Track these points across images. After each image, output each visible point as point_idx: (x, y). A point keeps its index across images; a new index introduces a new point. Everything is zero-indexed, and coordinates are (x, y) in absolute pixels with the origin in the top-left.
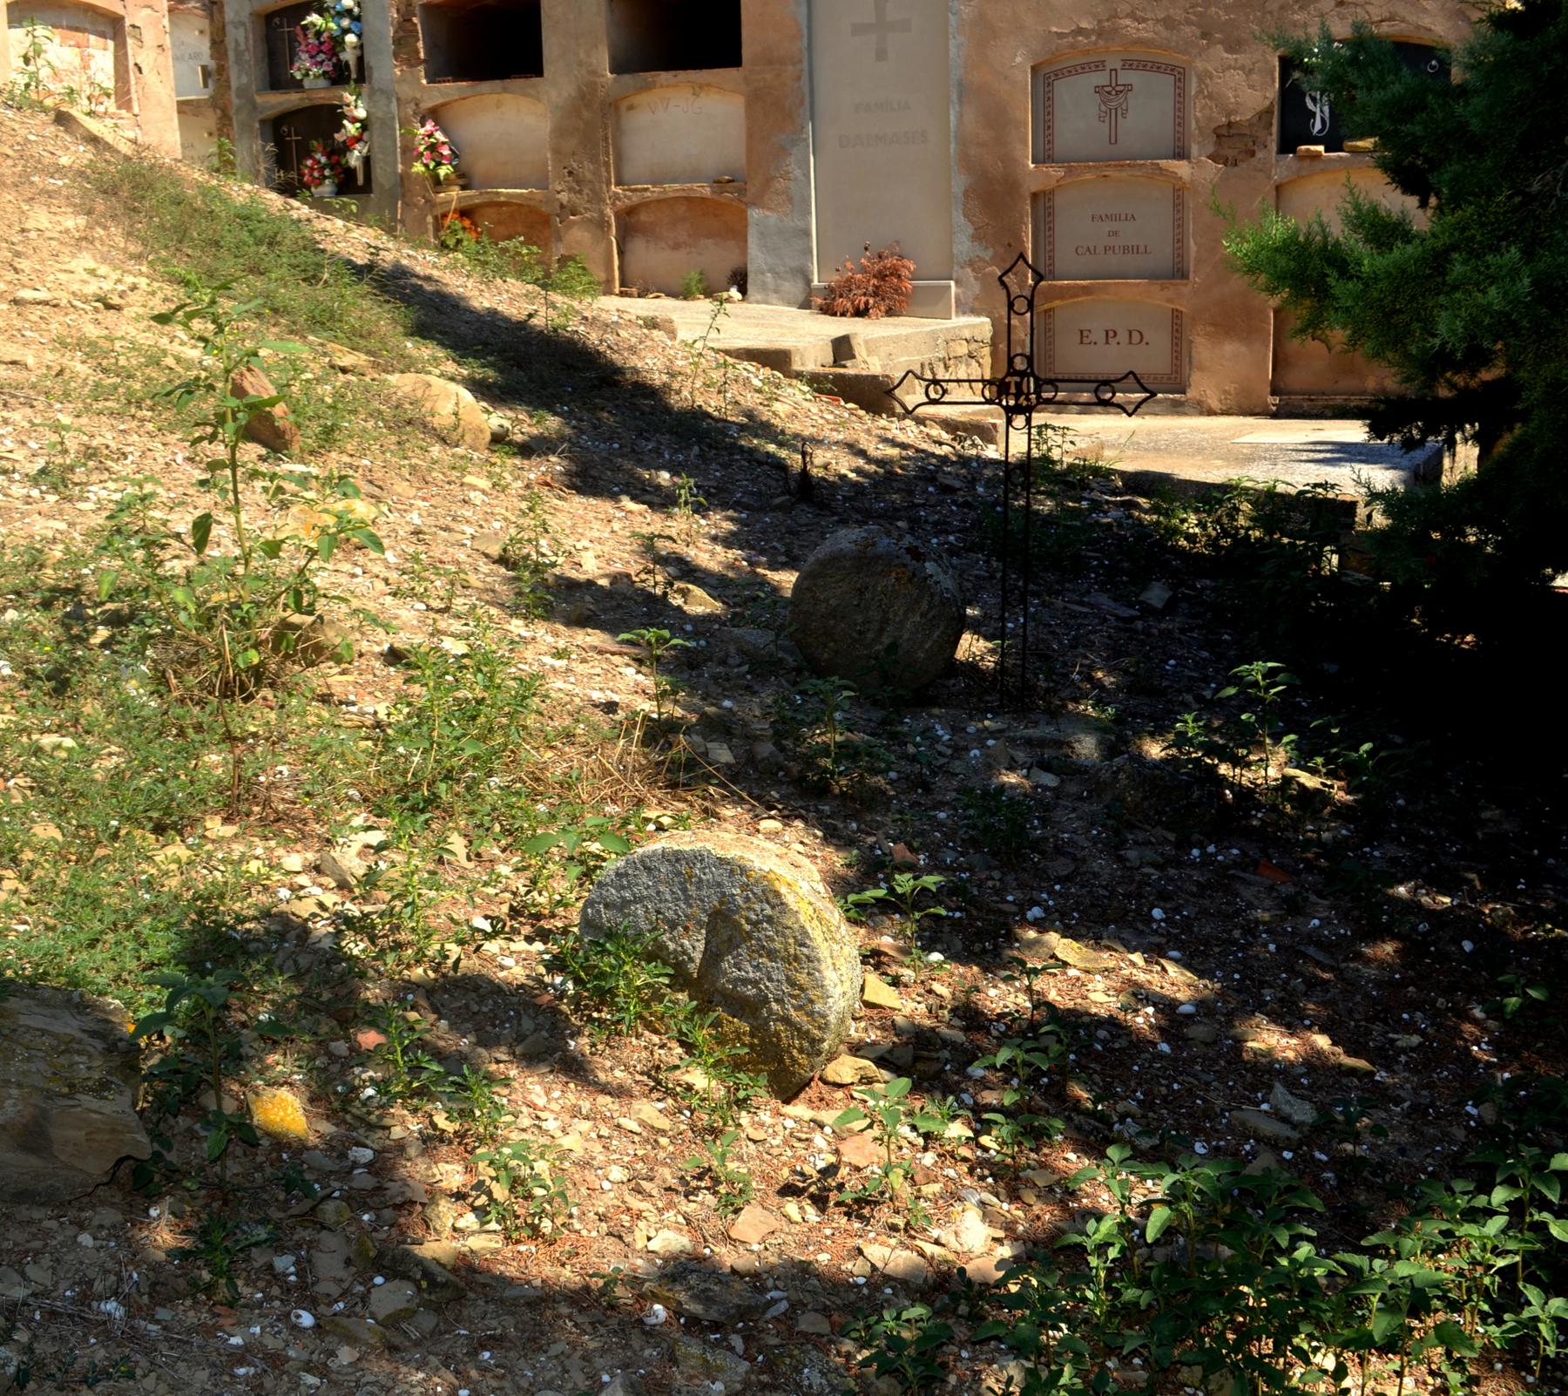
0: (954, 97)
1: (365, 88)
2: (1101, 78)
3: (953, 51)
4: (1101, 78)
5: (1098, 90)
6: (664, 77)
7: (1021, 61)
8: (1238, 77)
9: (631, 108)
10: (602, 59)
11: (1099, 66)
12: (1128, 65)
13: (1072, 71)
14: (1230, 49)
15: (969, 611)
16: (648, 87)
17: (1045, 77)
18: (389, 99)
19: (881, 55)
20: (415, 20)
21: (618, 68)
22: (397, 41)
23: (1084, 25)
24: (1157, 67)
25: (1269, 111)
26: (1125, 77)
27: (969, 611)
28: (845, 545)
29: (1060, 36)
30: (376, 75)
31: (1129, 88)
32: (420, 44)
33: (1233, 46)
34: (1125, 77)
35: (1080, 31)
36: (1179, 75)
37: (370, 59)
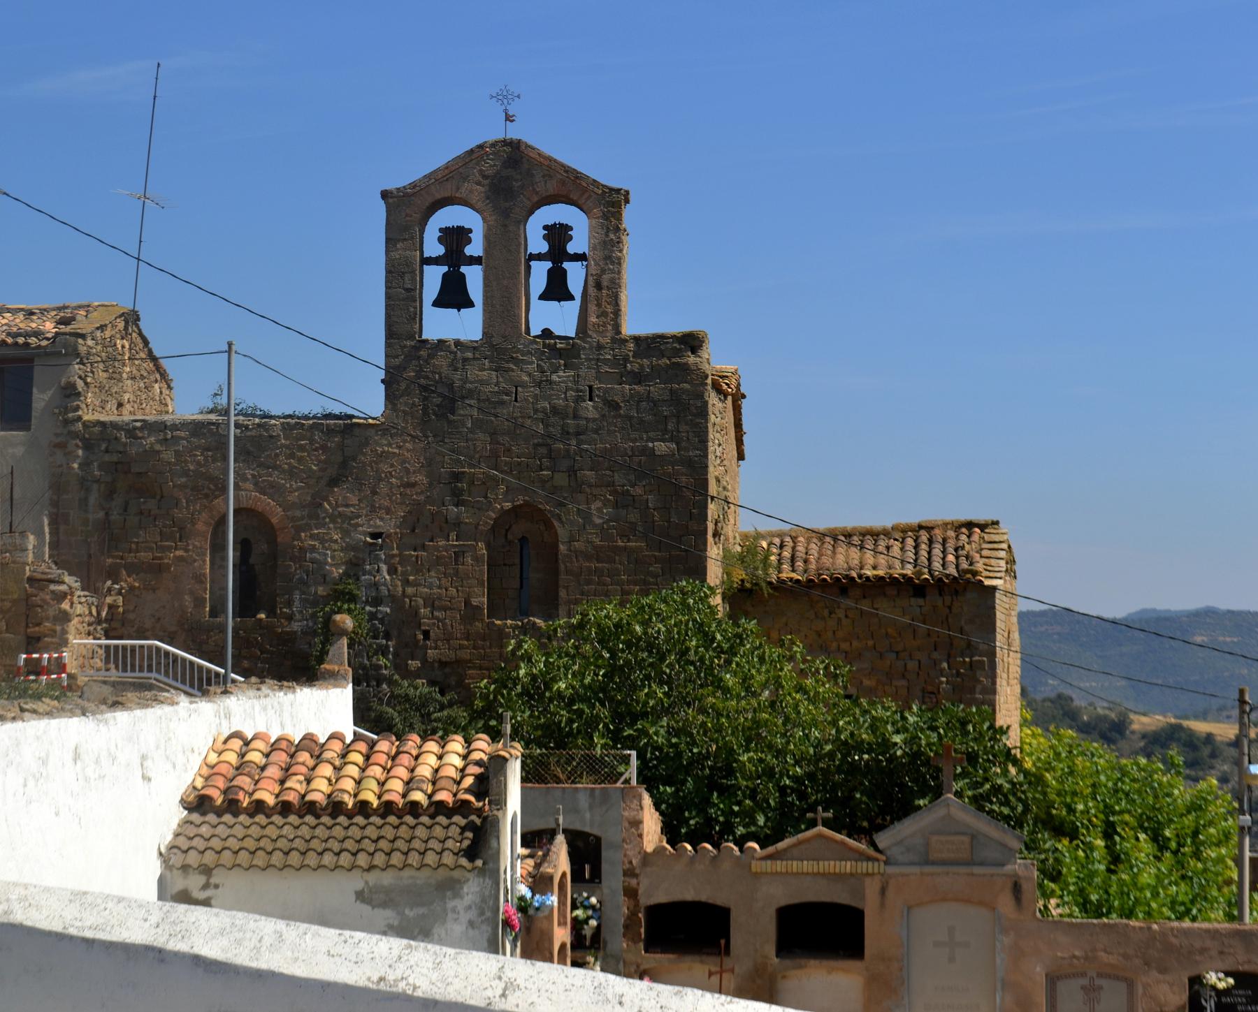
0: (999, 985)
1: (601, 954)
2: (1085, 982)
3: (998, 961)
4: (1085, 982)
5: (1083, 988)
6: (812, 962)
7: (1039, 971)
8: (1165, 987)
9: (784, 977)
10: (771, 950)
11: (1083, 975)
12: (1100, 975)
13: (1067, 976)
14: (1160, 972)
15: (388, 610)
16: (800, 967)
17: (1052, 980)
18: (618, 962)
19: (952, 959)
20: (640, 915)
21: (779, 952)
22: (626, 927)
23: (1077, 953)
24: (1117, 978)
25: (1184, 1007)
26: (1098, 982)
27: (388, 610)
28: (295, 628)
29: (1063, 958)
30: (609, 946)
31: (1101, 988)
32: (643, 930)
33: (1163, 970)
34: (1098, 982)
35: (1074, 956)
36: (1131, 985)
37: (604, 934)
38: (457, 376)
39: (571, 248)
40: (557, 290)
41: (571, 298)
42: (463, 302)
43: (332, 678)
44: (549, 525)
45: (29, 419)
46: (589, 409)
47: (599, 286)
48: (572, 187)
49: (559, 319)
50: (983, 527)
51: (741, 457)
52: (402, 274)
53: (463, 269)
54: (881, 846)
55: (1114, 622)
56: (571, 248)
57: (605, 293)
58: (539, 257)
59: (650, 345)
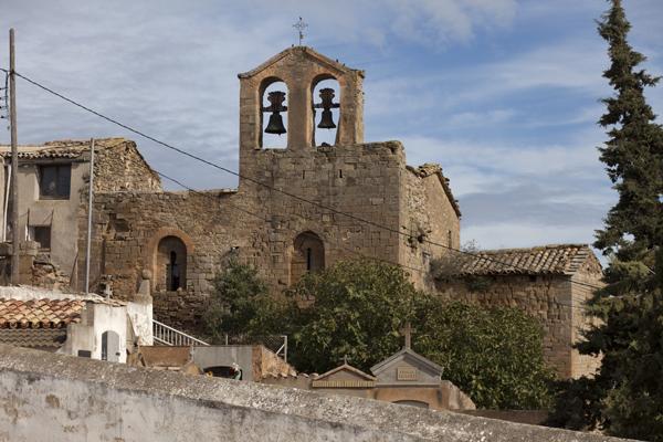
38: (275, 167)
39: (334, 101)
40: (327, 122)
41: (334, 126)
42: (281, 131)
43: (142, 301)
44: (322, 244)
45: (69, 193)
46: (341, 182)
47: (345, 120)
48: (332, 70)
49: (326, 136)
50: (579, 247)
51: (458, 214)
52: (248, 116)
53: (281, 113)
54: (374, 373)
55: (201, 194)
56: (334, 101)
57: (350, 120)
58: (318, 106)
59: (371, 148)
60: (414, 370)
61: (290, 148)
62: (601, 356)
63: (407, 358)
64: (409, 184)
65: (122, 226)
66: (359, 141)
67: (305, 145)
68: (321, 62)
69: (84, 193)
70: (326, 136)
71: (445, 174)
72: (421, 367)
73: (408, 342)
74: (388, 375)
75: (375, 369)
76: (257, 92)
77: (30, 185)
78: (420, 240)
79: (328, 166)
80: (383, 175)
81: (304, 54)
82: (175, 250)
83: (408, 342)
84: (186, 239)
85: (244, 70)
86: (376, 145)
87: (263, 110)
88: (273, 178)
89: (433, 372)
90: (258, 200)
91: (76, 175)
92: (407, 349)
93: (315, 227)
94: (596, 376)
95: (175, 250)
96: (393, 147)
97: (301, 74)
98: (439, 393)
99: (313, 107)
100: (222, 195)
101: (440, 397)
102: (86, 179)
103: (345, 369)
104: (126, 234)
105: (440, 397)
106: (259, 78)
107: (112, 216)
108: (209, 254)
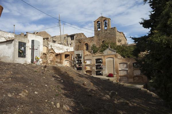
42: (100, 28)
49: (106, 28)
51: (126, 40)
57: (109, 25)
59: (112, 28)
60: (111, 51)
61: (101, 30)
62: (150, 28)
63: (109, 49)
64: (118, 34)
65: (80, 43)
66: (110, 28)
67: (103, 29)
68: (104, 18)
69: (76, 39)
70: (106, 28)
71: (124, 34)
72: (112, 51)
73: (109, 46)
74: (106, 53)
75: (104, 52)
76: (96, 23)
77: (69, 39)
78: (120, 41)
79: (106, 32)
80: (114, 32)
81: (102, 17)
82: (87, 45)
83: (109, 46)
84: (88, 43)
85: (94, 21)
86: (112, 28)
87: (97, 26)
88: (99, 34)
89: (114, 52)
90: (97, 37)
91: (75, 37)
92: (110, 48)
93: (105, 40)
94: (149, 34)
95: (87, 45)
96: (115, 28)
97: (102, 20)
98: (116, 55)
99: (104, 24)
100: (93, 37)
101: (116, 56)
102: (76, 37)
103: (98, 53)
104: (81, 44)
105: (116, 56)
106: (96, 21)
107: (79, 42)
108: (91, 44)
